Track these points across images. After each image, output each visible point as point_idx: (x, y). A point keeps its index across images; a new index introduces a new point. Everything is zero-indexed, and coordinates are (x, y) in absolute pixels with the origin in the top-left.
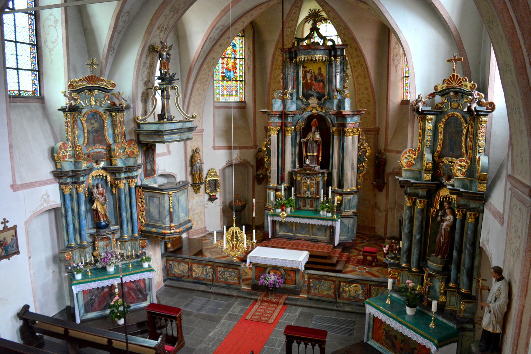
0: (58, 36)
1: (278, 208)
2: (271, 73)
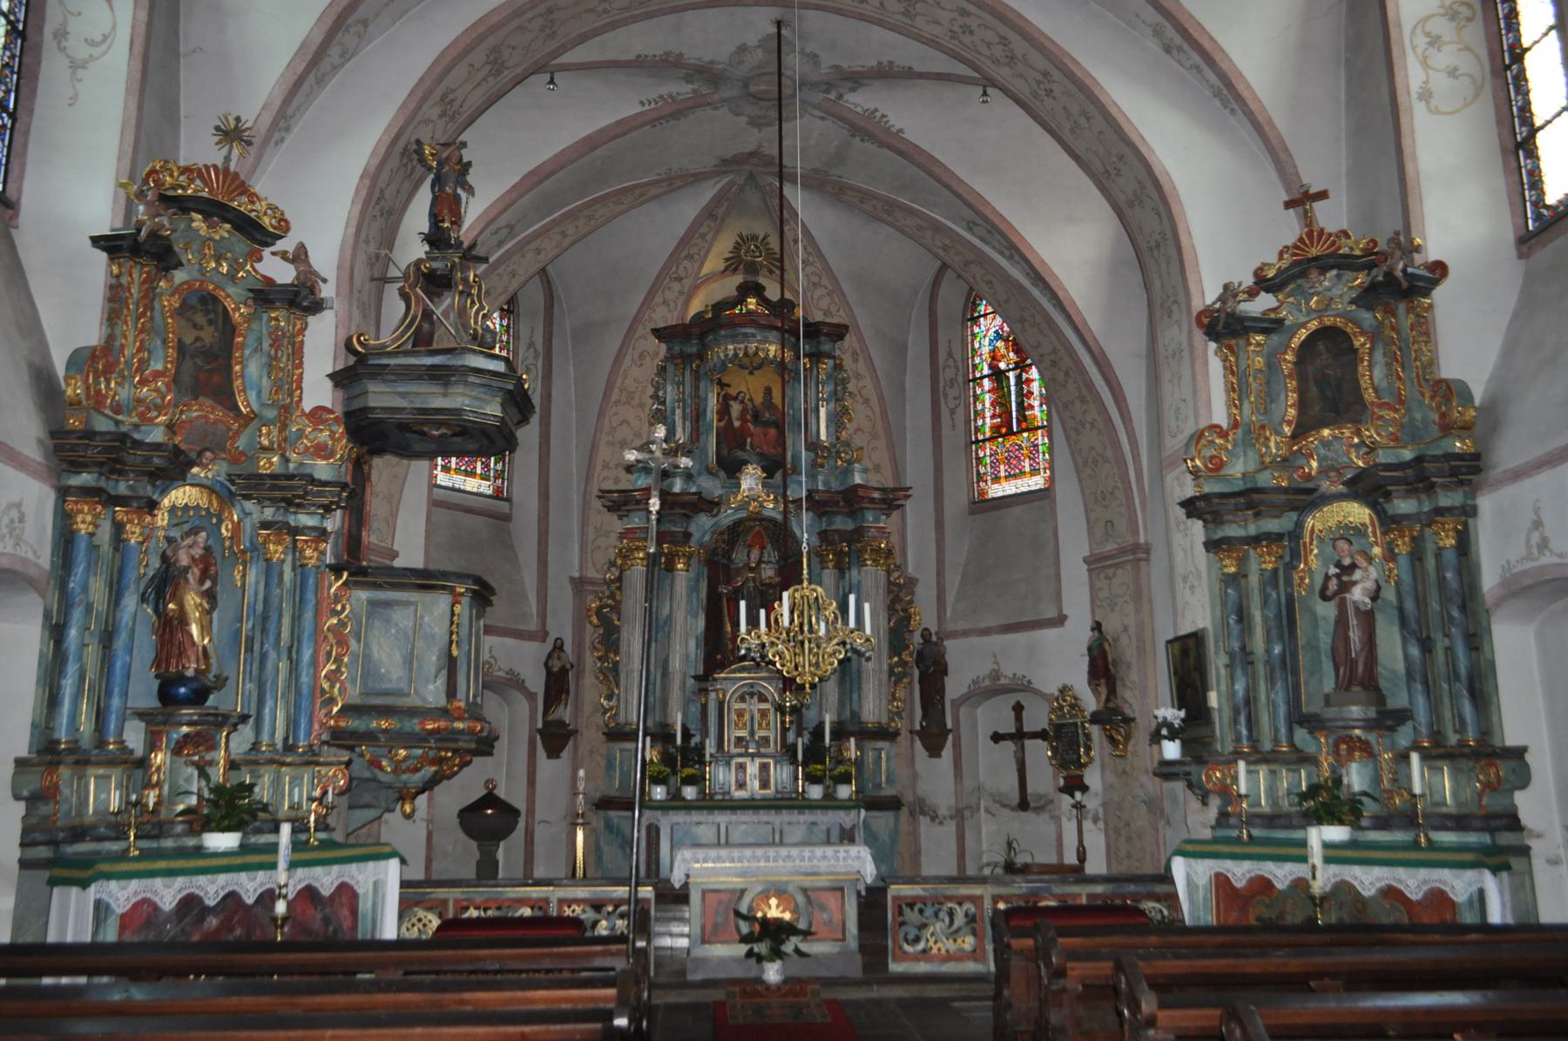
0: (114, 27)
2: (601, 414)
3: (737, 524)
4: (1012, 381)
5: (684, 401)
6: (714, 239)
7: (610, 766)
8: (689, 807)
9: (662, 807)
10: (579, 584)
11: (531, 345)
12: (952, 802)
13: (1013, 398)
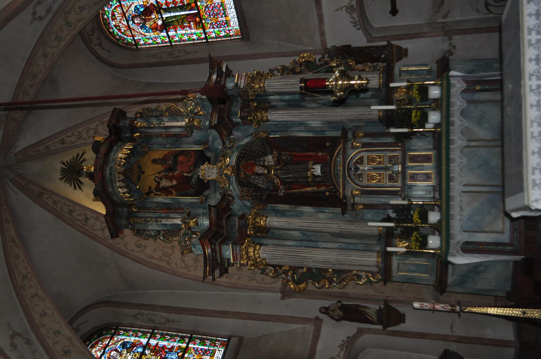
1: (338, 81)
2: (175, 274)
3: (241, 183)
4: (168, 15)
5: (157, 218)
6: (58, 195)
7: (410, 281)
8: (447, 217)
9: (447, 239)
10: (285, 294)
11: (135, 316)
12: (439, 39)
13: (178, 14)
